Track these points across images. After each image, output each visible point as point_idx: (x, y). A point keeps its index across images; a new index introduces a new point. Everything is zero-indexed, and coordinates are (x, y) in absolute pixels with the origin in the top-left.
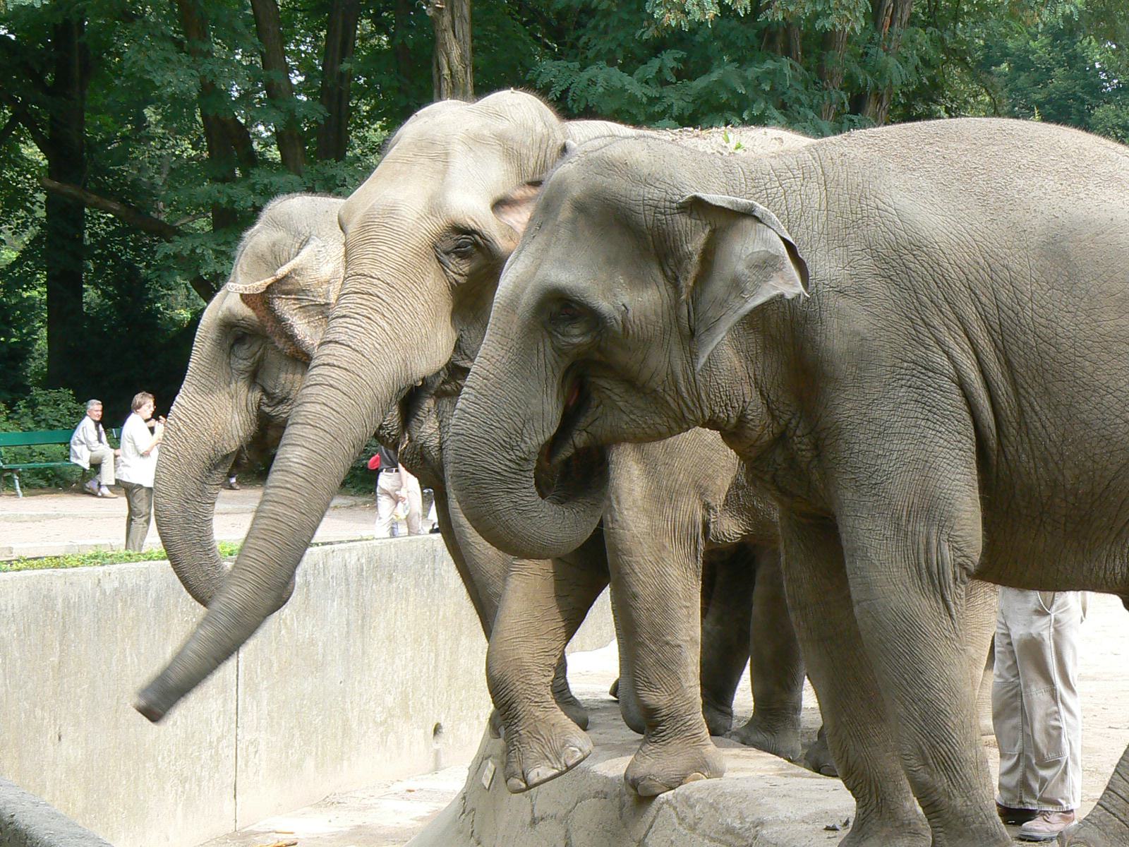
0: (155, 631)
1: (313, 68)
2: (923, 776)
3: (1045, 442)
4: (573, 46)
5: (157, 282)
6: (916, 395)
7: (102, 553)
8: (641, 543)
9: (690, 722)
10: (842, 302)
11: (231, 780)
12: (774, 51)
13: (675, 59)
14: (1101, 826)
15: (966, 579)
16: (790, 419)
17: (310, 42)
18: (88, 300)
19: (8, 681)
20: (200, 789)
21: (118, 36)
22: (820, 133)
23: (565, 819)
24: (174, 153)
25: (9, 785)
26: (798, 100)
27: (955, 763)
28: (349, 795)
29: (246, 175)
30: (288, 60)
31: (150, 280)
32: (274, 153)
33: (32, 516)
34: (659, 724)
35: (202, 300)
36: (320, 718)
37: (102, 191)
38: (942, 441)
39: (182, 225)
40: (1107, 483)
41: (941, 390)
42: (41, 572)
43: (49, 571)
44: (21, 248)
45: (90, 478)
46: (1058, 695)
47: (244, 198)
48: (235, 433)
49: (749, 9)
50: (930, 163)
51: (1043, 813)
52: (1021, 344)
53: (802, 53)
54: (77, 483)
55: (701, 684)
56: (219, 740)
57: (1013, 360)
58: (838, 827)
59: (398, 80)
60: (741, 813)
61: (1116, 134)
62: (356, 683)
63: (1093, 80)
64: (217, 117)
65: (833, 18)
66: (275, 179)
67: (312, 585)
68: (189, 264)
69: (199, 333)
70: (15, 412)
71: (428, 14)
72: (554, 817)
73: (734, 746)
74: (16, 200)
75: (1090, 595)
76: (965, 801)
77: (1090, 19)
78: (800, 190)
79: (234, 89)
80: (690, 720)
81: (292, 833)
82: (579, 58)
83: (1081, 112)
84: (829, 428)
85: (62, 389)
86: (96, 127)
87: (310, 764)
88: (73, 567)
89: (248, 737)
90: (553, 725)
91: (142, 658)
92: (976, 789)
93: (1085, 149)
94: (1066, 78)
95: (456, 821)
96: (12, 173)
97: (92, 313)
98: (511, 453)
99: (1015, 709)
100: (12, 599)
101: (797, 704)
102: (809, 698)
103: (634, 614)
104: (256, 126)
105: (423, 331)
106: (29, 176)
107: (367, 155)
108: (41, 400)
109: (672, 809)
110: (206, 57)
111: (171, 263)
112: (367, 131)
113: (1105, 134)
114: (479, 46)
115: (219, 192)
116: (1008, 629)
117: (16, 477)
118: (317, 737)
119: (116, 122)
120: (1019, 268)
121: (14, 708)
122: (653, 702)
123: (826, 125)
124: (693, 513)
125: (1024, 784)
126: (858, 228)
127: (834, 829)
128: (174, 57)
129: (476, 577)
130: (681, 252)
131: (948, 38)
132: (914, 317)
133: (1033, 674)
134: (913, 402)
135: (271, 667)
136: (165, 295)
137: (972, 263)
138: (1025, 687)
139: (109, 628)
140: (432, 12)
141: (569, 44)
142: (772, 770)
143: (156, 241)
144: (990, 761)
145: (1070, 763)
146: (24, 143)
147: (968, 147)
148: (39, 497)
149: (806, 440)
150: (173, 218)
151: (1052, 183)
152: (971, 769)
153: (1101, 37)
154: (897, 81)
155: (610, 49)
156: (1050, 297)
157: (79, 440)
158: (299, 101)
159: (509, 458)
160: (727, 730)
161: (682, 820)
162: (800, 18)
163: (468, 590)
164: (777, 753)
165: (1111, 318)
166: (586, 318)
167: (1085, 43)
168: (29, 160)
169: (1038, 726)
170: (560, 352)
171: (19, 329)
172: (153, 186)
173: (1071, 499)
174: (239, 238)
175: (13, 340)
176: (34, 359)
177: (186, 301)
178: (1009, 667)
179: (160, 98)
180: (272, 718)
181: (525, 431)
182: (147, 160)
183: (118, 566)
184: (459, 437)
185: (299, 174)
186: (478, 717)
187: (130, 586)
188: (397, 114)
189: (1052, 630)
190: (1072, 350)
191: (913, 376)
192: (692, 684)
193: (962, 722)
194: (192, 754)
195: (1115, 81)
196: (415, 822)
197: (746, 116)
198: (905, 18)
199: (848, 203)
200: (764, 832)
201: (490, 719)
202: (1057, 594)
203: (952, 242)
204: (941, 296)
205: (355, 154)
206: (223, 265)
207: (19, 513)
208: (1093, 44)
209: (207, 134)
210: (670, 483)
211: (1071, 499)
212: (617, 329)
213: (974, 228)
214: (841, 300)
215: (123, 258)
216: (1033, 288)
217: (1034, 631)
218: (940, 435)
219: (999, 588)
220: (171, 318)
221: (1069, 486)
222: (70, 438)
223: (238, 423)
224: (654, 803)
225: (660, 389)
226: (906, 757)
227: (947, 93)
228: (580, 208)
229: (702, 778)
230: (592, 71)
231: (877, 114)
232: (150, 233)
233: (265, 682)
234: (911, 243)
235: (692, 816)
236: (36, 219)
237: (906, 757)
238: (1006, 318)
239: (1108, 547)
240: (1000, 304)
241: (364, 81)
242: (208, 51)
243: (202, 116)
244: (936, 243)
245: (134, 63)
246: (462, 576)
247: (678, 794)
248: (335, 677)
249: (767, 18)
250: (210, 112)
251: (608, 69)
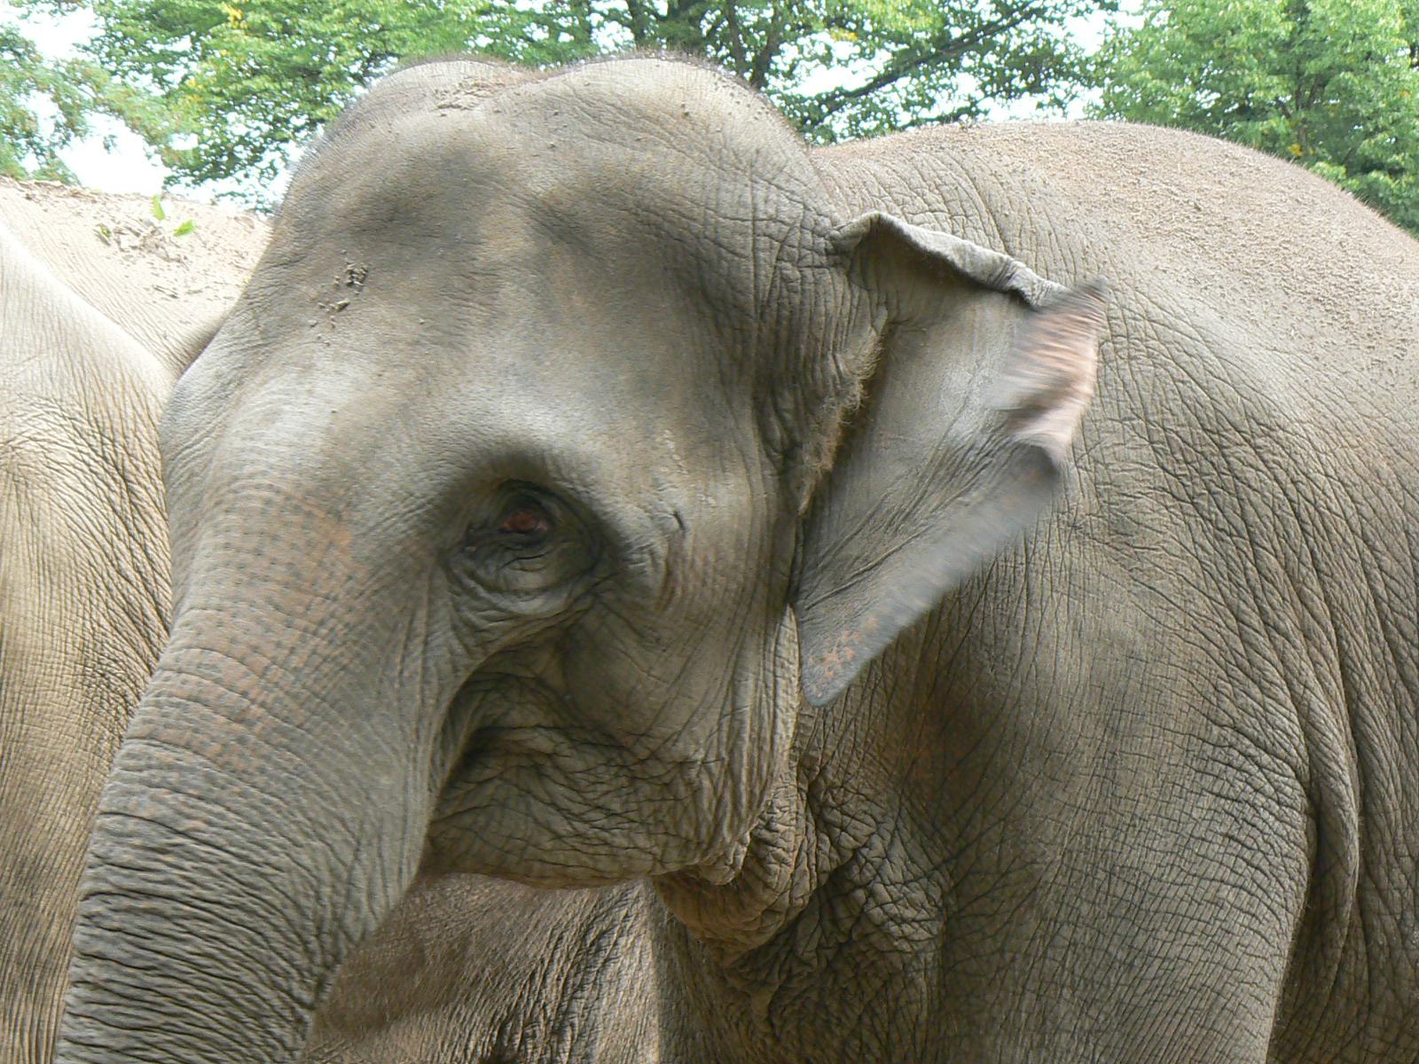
130: (819, 375)
137: (1367, 474)
210: (28, 946)
225: (1063, 708)
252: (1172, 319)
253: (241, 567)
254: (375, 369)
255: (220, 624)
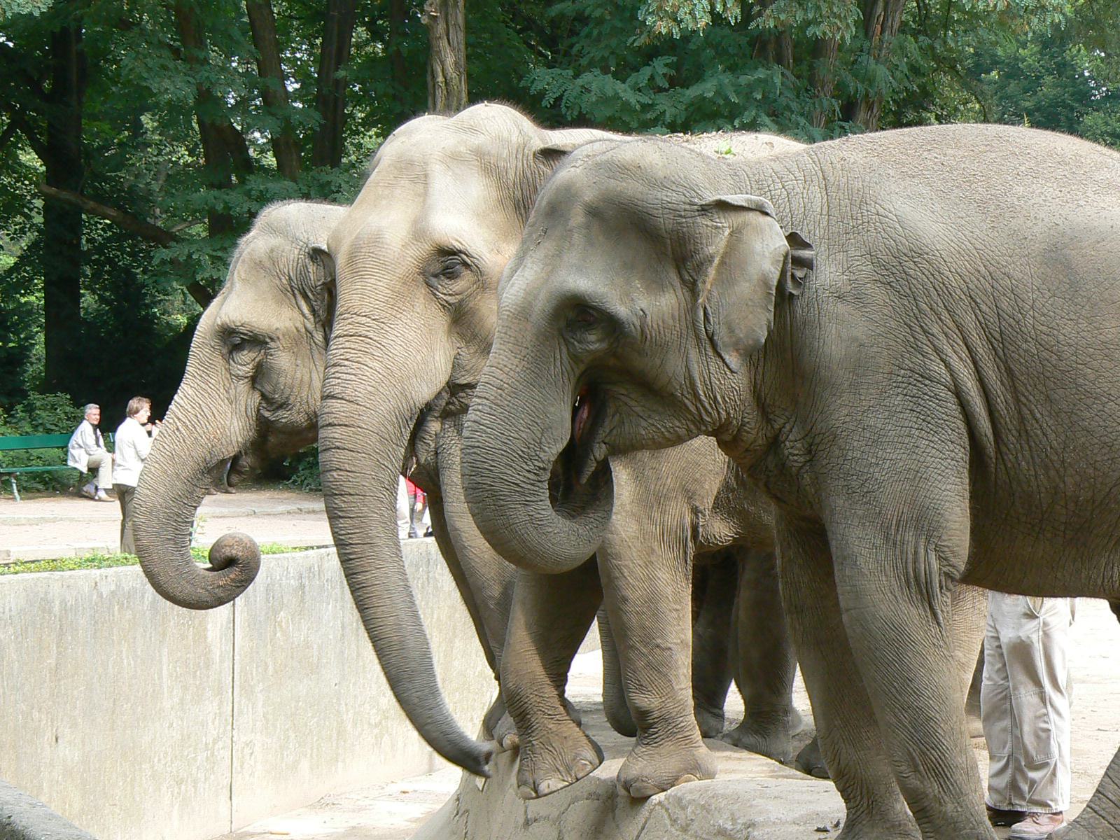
0: (151, 633)
1: (309, 75)
2: (914, 782)
3: (1046, 449)
4: (567, 54)
5: (154, 287)
6: (911, 404)
7: (99, 556)
8: (629, 547)
9: (682, 724)
10: (841, 308)
11: (226, 782)
12: (766, 59)
13: (666, 65)
14: (1090, 828)
15: (951, 586)
16: (785, 424)
17: (306, 50)
18: (85, 305)
19: (5, 683)
20: (196, 790)
21: (116, 43)
22: (812, 140)
23: (558, 821)
24: (170, 159)
25: (6, 787)
26: (788, 108)
27: (945, 770)
28: (343, 796)
29: (242, 181)
30: (283, 67)
31: (147, 286)
32: (270, 160)
33: (29, 519)
34: (651, 726)
35: (199, 306)
36: (315, 720)
37: (101, 198)
38: (934, 451)
39: (178, 231)
40: (1108, 490)
41: (937, 399)
42: (38, 575)
43: (46, 574)
44: (19, 254)
45: (87, 482)
46: (1047, 698)
47: (238, 202)
48: (234, 439)
49: (739, 18)
50: (929, 170)
51: (1033, 815)
52: (1022, 353)
53: (794, 60)
54: (74, 486)
55: (693, 686)
56: (214, 743)
57: (1014, 368)
58: (828, 828)
59: (393, 87)
60: (732, 814)
61: (1105, 141)
62: (351, 685)
63: (1082, 87)
64: (213, 124)
65: (824, 27)
66: (270, 185)
67: (307, 588)
68: (186, 269)
69: (197, 339)
70: (13, 416)
71: (423, 22)
72: (547, 818)
73: (726, 749)
74: (15, 205)
75: (1080, 601)
76: (956, 807)
77: (1079, 28)
78: (802, 193)
79: (230, 96)
80: (682, 722)
81: (287, 834)
82: (573, 65)
83: (1069, 120)
84: (824, 434)
85: (59, 394)
86: (93, 133)
87: (305, 765)
88: (70, 570)
89: (243, 739)
90: (565, 738)
91: (139, 660)
92: (966, 795)
93: (1081, 156)
94: (1055, 86)
95: (450, 823)
96: (9, 180)
97: (90, 318)
98: (529, 463)
99: (1005, 711)
100: (9, 602)
101: (787, 705)
102: (800, 699)
103: (625, 618)
104: (252, 133)
105: (419, 357)
106: (27, 182)
107: (362, 162)
108: (38, 404)
109: (664, 811)
110: (202, 65)
111: (168, 268)
112: (363, 138)
113: (1095, 140)
114: (473, 53)
115: (215, 198)
116: (997, 631)
117: (13, 481)
118: (313, 739)
119: (113, 129)
120: (1020, 276)
121: (11, 710)
122: (646, 705)
123: (817, 132)
124: (682, 517)
125: (1014, 786)
126: (858, 234)
127: (825, 830)
128: (171, 65)
129: (471, 580)
131: (938, 47)
132: (912, 324)
133: (1021, 677)
134: (908, 411)
135: (266, 670)
136: (161, 300)
137: (973, 271)
138: (1014, 690)
139: (106, 631)
140: (427, 20)
141: (562, 52)
142: (763, 772)
143: (152, 247)
144: (979, 763)
145: (1059, 765)
146: (22, 149)
147: (966, 154)
148: (36, 500)
149: (799, 445)
150: (169, 223)
151: (1051, 190)
152: (961, 775)
153: (1090, 47)
154: (886, 92)
155: (603, 57)
156: (1052, 305)
157: (79, 445)
158: (295, 108)
159: (527, 468)
160: (718, 732)
161: (674, 821)
162: (792, 27)
163: (461, 594)
164: (769, 756)
165: (1112, 325)
166: (602, 325)
167: (1074, 51)
168: (26, 167)
169: (1027, 728)
170: (575, 358)
171: (17, 334)
172: (150, 192)
173: (1071, 506)
174: (235, 245)
175: (11, 345)
176: (32, 364)
177: (182, 306)
178: (999, 670)
179: (157, 105)
180: (267, 720)
181: (543, 440)
182: (144, 166)
183: (114, 569)
184: (475, 450)
185: (295, 180)
186: (472, 719)
187: (126, 589)
188: (389, 120)
189: (1041, 633)
190: (1074, 358)
191: (910, 384)
192: (683, 686)
193: (952, 729)
194: (188, 756)
195: (1104, 89)
196: (409, 823)
197: (736, 123)
198: (896, 26)
199: (848, 209)
200: (756, 833)
201: (484, 721)
202: (1045, 599)
203: (952, 250)
204: (941, 304)
205: (350, 161)
206: (219, 270)
207: (16, 516)
208: (1082, 51)
209: (204, 140)
210: (657, 487)
211: (1071, 506)
212: (635, 334)
213: (975, 236)
214: (839, 305)
215: (120, 263)
216: (1035, 296)
217: (1023, 634)
218: (932, 445)
219: (990, 593)
220: (167, 323)
221: (1069, 494)
222: (68, 442)
223: (237, 428)
224: (647, 804)
226: (896, 764)
227: (937, 100)
228: (594, 213)
229: (694, 780)
230: (586, 77)
231: (868, 121)
232: (146, 238)
233: (261, 684)
234: (911, 250)
235: (684, 816)
236: (34, 224)
237: (896, 764)
238: (1007, 326)
239: (1107, 554)
240: (1001, 312)
241: (360, 88)
242: (205, 59)
243: (199, 122)
244: (937, 250)
245: (131, 70)
246: (455, 579)
247: (670, 795)
248: (330, 679)
249: (758, 26)
250: (208, 121)
251: (601, 77)
252: (887, 213)
253: (501, 338)
254: (542, 266)
255: (495, 358)
